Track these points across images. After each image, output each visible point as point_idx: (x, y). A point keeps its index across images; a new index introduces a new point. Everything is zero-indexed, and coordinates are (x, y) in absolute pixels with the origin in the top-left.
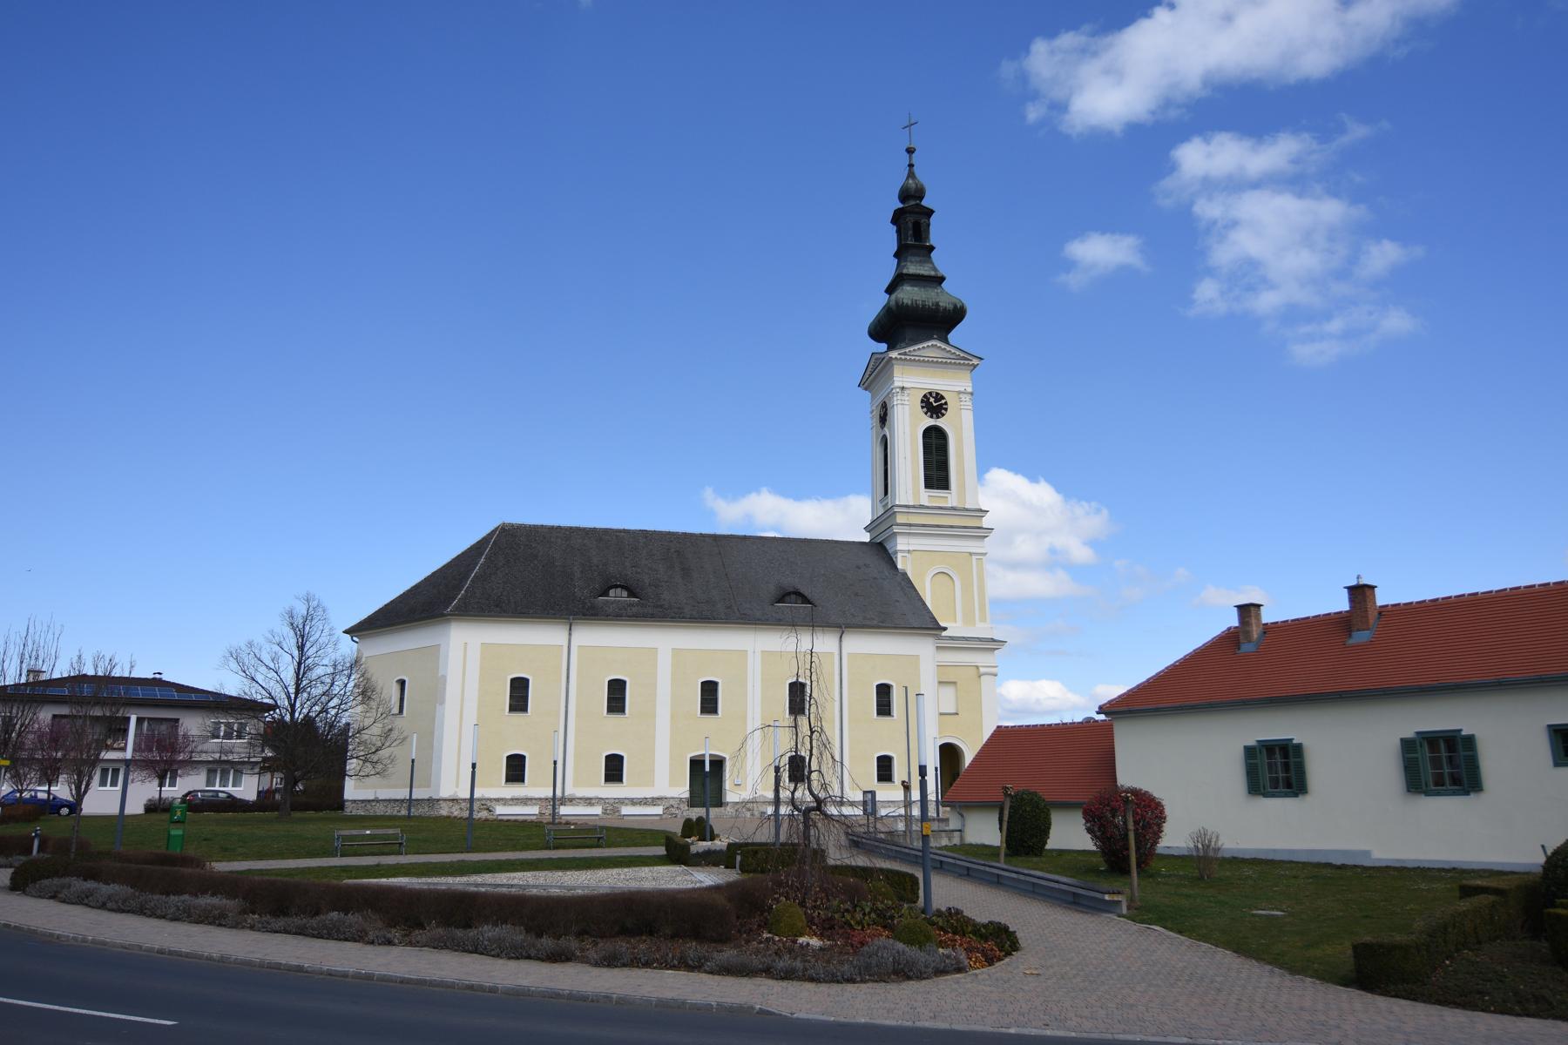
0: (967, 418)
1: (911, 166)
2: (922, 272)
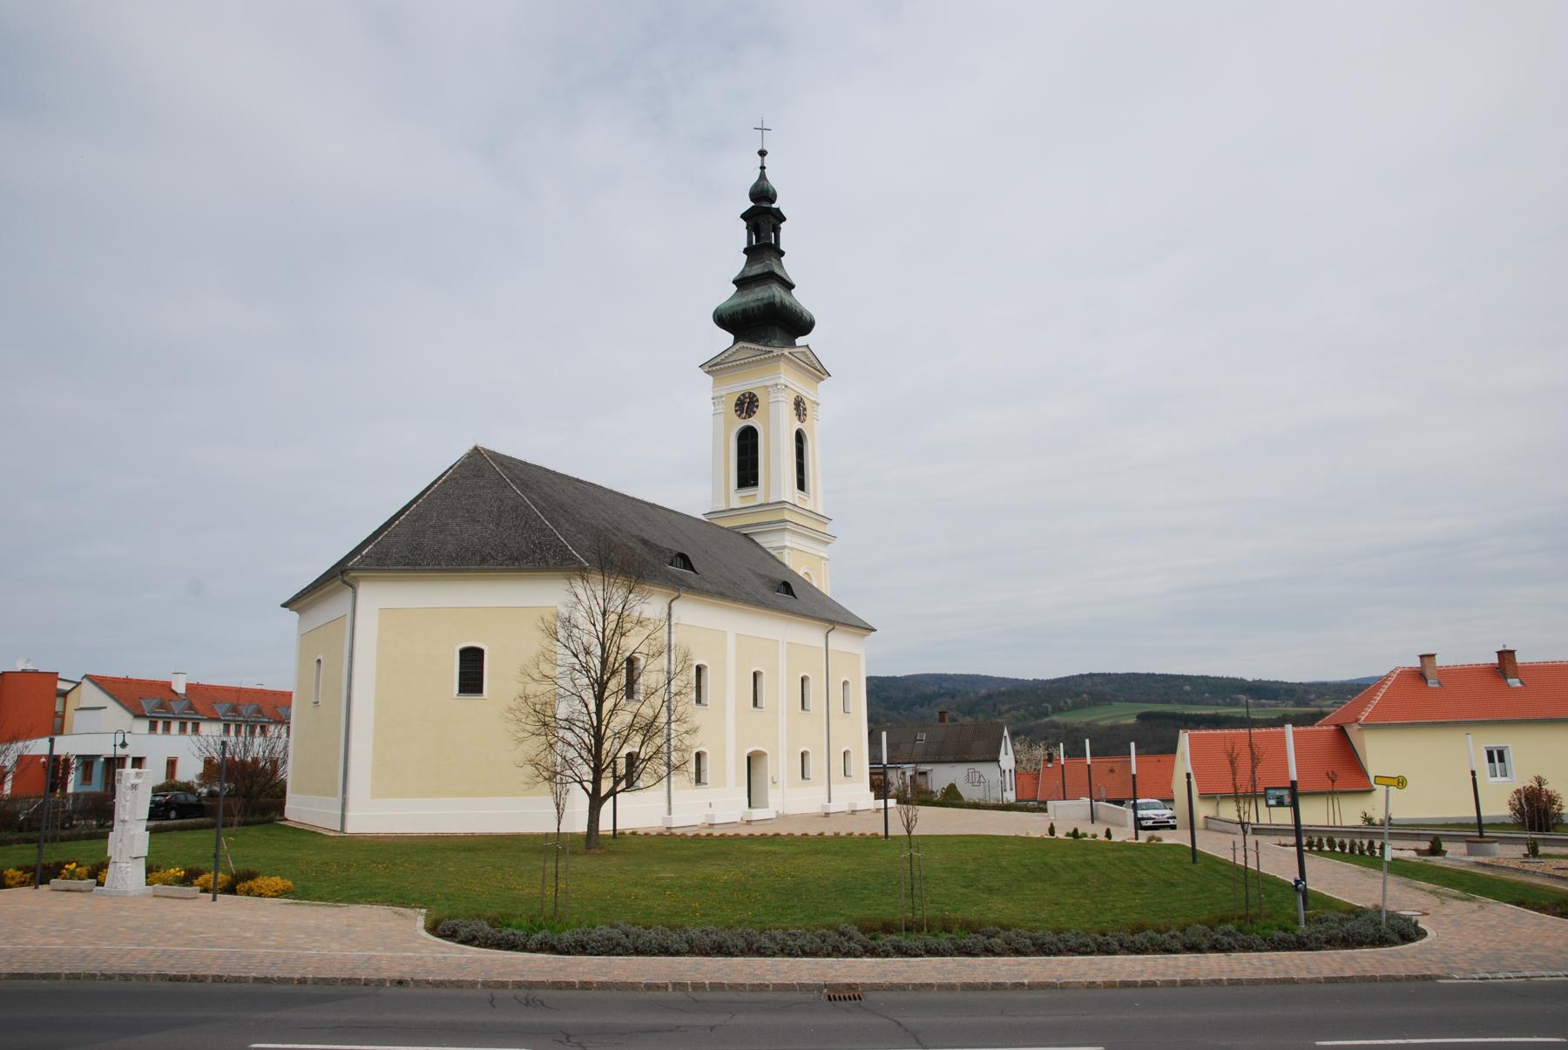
1: (763, 168)
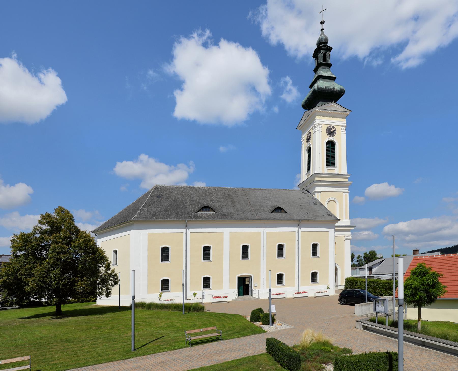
0: (344, 137)
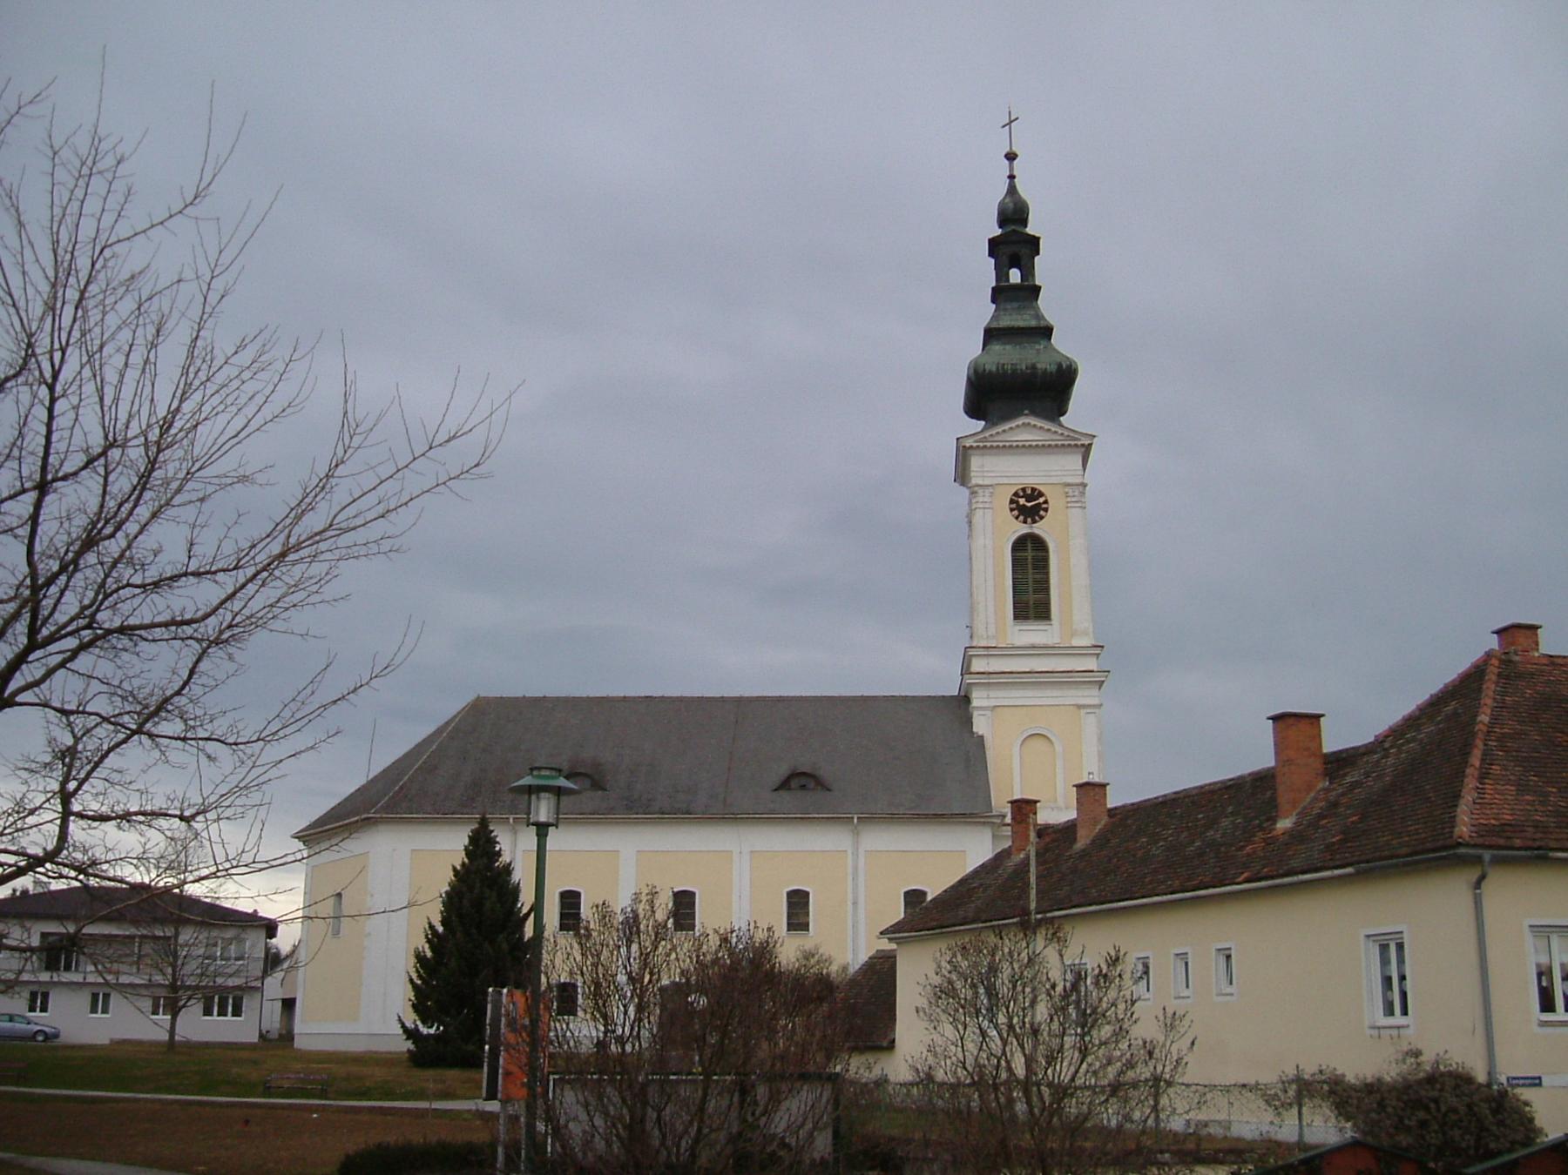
1: (1012, 177)
2: (1021, 324)
